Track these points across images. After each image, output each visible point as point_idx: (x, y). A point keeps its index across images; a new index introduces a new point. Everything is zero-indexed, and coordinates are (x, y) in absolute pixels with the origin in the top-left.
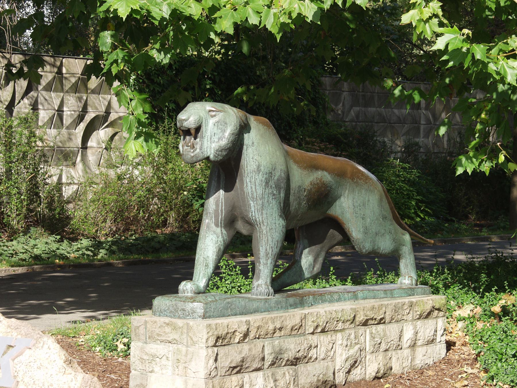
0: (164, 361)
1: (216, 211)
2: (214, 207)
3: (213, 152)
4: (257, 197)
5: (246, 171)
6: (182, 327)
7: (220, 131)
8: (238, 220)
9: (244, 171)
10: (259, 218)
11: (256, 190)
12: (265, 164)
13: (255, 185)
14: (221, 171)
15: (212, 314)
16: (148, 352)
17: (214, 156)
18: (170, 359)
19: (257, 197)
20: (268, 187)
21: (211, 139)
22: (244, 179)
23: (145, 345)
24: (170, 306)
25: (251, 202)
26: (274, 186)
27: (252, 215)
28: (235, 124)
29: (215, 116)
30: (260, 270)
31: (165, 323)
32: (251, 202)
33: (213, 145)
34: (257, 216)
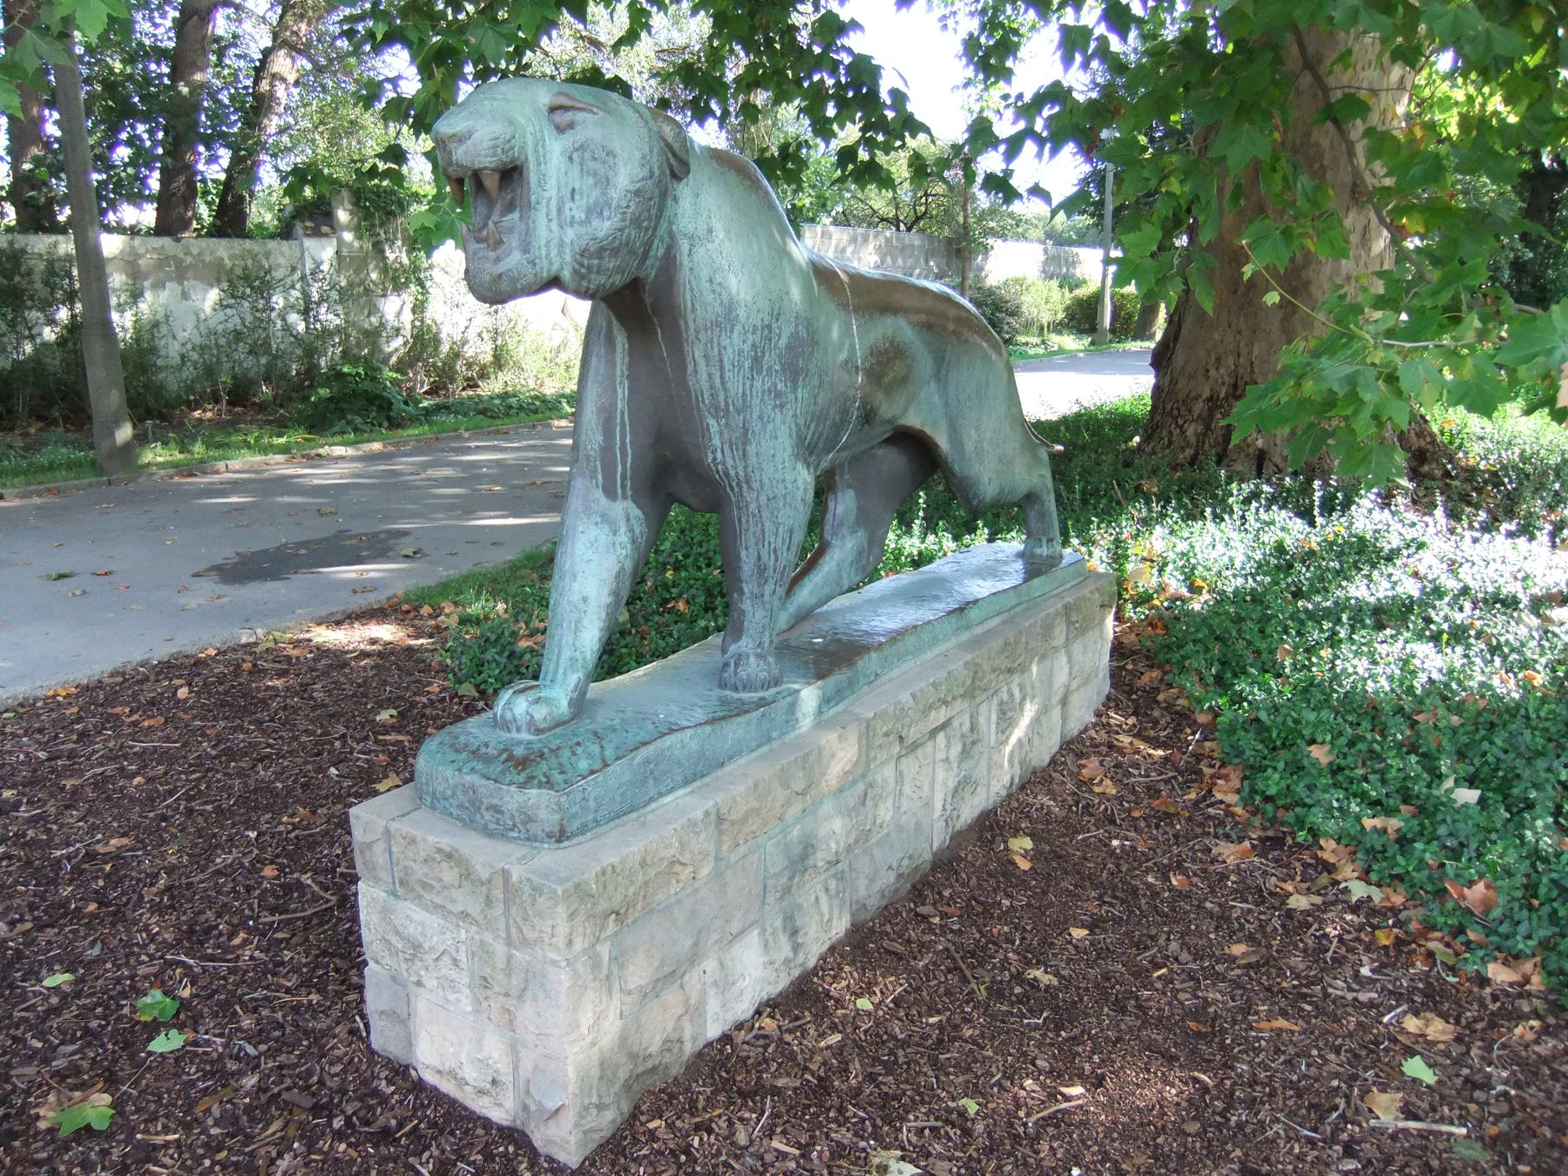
0: (446, 967)
1: (607, 451)
2: (600, 438)
3: (568, 258)
4: (727, 404)
5: (692, 326)
6: (489, 881)
7: (591, 181)
8: (583, 1079)
9: (686, 323)
10: (735, 467)
11: (723, 383)
12: (749, 298)
13: (722, 369)
14: (615, 322)
15: (590, 817)
16: (400, 929)
17: (576, 272)
18: (464, 966)
19: (727, 404)
20: (759, 372)
21: (560, 211)
22: (687, 348)
23: (392, 900)
24: (456, 786)
25: (712, 422)
26: (777, 367)
27: (715, 459)
28: (643, 157)
29: (571, 126)
30: (744, 612)
31: (440, 850)
32: (712, 422)
33: (570, 234)
34: (730, 463)
